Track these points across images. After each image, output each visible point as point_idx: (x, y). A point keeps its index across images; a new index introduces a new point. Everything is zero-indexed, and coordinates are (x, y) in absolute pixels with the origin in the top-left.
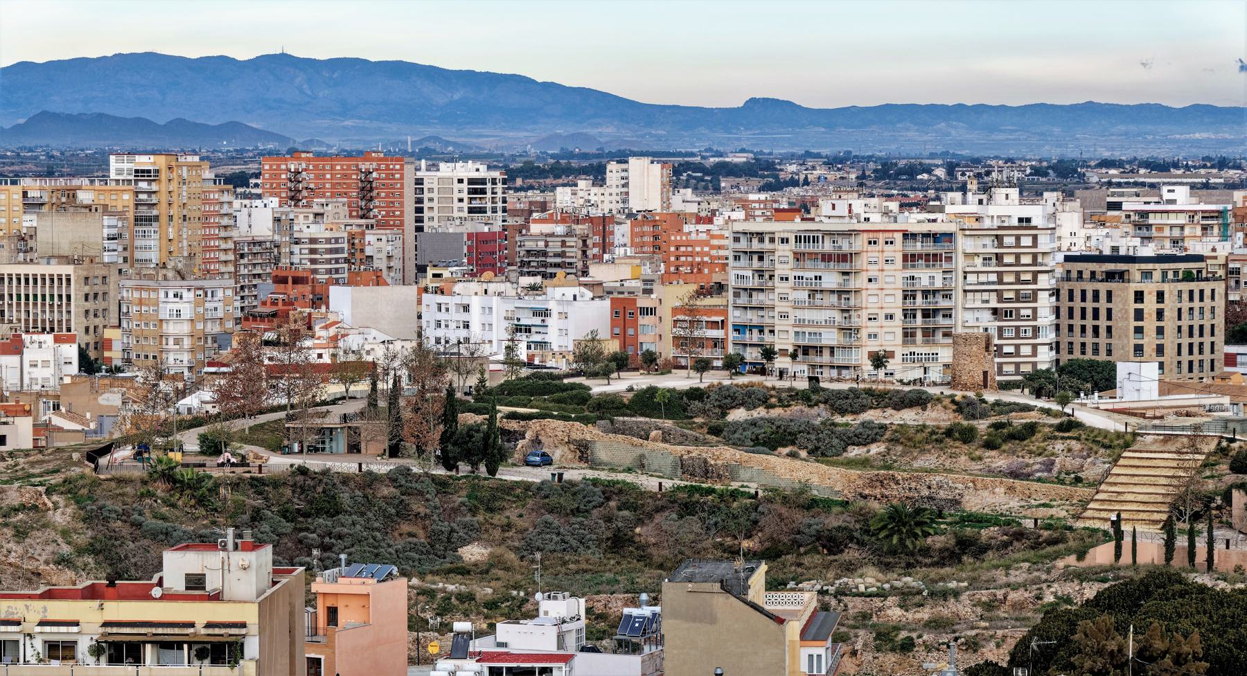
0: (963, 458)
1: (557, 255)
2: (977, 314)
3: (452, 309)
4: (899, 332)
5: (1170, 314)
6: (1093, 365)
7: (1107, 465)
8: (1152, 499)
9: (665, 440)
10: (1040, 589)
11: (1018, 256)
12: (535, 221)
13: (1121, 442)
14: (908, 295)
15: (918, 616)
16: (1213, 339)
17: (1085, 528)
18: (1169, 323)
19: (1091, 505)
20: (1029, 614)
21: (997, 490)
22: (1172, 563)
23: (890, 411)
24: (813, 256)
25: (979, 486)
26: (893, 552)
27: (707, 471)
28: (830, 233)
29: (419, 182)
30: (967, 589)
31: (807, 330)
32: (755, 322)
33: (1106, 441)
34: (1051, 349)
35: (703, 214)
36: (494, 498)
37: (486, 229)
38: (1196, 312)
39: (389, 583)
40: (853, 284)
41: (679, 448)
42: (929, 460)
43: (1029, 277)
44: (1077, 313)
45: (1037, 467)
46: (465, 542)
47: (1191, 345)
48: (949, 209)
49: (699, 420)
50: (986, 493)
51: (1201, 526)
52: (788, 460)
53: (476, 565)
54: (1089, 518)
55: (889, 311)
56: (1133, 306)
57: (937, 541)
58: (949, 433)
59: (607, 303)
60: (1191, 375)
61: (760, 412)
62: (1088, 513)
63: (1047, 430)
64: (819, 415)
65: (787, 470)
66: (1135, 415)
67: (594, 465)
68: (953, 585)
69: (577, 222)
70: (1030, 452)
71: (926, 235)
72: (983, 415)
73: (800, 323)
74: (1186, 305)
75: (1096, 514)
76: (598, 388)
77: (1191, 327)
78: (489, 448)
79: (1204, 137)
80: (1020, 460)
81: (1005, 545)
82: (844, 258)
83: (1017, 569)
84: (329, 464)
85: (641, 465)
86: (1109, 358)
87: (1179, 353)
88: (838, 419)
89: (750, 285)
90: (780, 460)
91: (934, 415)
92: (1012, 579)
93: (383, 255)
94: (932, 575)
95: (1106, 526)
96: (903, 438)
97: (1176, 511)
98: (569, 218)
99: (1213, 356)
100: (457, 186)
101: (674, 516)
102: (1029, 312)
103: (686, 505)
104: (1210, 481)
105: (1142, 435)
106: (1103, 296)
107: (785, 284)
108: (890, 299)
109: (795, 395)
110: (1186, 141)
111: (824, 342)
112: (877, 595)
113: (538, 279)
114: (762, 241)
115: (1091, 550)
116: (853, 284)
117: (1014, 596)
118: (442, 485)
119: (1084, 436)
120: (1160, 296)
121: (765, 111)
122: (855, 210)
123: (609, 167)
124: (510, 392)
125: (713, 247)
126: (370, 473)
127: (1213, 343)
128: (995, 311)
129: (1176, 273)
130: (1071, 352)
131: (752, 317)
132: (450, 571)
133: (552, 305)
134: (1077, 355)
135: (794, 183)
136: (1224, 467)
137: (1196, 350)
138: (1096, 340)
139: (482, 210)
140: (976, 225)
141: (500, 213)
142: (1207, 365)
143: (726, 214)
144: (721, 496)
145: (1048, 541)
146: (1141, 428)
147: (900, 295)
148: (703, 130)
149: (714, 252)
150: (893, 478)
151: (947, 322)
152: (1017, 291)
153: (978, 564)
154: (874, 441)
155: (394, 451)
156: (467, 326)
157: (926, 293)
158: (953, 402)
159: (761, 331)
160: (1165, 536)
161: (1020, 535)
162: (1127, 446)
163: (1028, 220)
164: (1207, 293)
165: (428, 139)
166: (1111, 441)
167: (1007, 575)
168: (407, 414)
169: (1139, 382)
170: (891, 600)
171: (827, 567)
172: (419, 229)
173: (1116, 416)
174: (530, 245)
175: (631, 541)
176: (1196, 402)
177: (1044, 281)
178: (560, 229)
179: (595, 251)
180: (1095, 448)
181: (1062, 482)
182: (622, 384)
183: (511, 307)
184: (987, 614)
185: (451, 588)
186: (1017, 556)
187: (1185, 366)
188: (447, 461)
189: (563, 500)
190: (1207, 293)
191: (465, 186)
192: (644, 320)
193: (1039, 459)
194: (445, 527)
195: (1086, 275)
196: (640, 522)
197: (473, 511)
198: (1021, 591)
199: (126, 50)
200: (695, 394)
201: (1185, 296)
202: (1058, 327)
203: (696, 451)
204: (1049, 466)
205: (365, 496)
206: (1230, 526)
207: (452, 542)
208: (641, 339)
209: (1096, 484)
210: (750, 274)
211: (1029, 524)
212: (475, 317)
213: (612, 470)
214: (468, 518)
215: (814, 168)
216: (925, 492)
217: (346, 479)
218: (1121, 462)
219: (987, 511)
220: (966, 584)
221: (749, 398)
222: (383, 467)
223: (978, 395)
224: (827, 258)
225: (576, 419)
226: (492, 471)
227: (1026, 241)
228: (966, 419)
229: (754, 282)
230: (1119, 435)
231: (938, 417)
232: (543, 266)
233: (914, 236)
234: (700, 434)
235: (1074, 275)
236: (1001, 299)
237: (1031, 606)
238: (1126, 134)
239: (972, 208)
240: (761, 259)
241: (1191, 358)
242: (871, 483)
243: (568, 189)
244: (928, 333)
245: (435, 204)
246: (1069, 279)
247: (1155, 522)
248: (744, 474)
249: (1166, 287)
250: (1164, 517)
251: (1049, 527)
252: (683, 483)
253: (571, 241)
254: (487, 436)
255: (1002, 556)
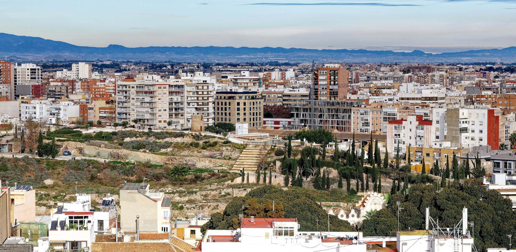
0: (196, 152)
1: (58, 92)
2: (191, 109)
3: (31, 108)
4: (168, 115)
5: (247, 109)
8: (252, 164)
9: (105, 147)
11: (203, 92)
12: (52, 81)
14: (171, 104)
15: (184, 199)
18: (247, 112)
23: (173, 138)
24: (142, 92)
26: (176, 180)
27: (119, 157)
28: (147, 85)
29: (15, 69)
31: (140, 114)
32: (124, 112)
35: (102, 79)
36: (54, 165)
37: (37, 84)
38: (255, 109)
39: (30, 191)
40: (154, 100)
41: (110, 150)
42: (186, 153)
43: (206, 98)
44: (220, 109)
46: (46, 179)
47: (254, 118)
48: (182, 78)
49: (116, 141)
52: (143, 153)
53: (49, 185)
55: (165, 109)
56: (237, 107)
57: (189, 177)
58: (191, 144)
59: (78, 106)
61: (134, 139)
64: (152, 139)
65: (143, 156)
67: (84, 155)
68: (195, 190)
69: (65, 82)
70: (216, 150)
71: (175, 86)
72: (201, 139)
73: (138, 112)
74: (252, 106)
76: (84, 132)
77: (254, 113)
78: (50, 150)
79: (246, 57)
81: (210, 178)
82: (151, 93)
84: (4, 155)
85: (98, 155)
88: (158, 141)
89: (123, 101)
90: (141, 153)
91: (186, 139)
92: (212, 188)
93: (5, 92)
94: (188, 187)
95: (239, 172)
96: (177, 146)
98: (62, 80)
100: (27, 71)
101: (110, 170)
102: (206, 109)
103: (113, 167)
106: (228, 104)
107: (133, 100)
108: (165, 105)
109: (144, 134)
110: (240, 58)
111: (145, 118)
112: (172, 193)
113: (54, 99)
114: (126, 87)
116: (154, 100)
118: (38, 161)
120: (245, 104)
121: (114, 48)
122: (154, 78)
123: (73, 65)
124: (58, 133)
125: (107, 89)
126: (16, 158)
128: (196, 108)
129: (249, 97)
131: (123, 110)
132: (42, 187)
133: (61, 107)
134: (220, 121)
135: (125, 70)
136: (273, 154)
137: (255, 120)
139: (35, 78)
140: (190, 83)
141: (40, 79)
143: (109, 80)
144: (124, 164)
145: (222, 177)
147: (168, 104)
148: (96, 54)
149: (107, 91)
150: (175, 158)
151: (182, 112)
152: (203, 102)
154: (169, 147)
155: (23, 151)
156: (35, 113)
157: (176, 103)
158: (192, 135)
159: (126, 115)
161: (214, 175)
162: (244, 148)
163: (206, 81)
164: (258, 103)
165: (12, 57)
168: (26, 140)
169: (242, 129)
170: (176, 195)
171: (157, 185)
172: (15, 84)
174: (51, 89)
175: (96, 178)
177: (211, 100)
178: (59, 84)
179: (70, 90)
182: (92, 131)
183: (49, 107)
185: (42, 192)
187: (252, 124)
188: (40, 155)
189: (77, 166)
190: (258, 103)
191: (29, 71)
192: (89, 111)
193: (218, 152)
194: (40, 174)
195: (223, 98)
196: (99, 172)
197: (48, 169)
198: (215, 191)
199: (27, 35)
200: (114, 134)
201: (252, 104)
202: (214, 113)
203: (115, 151)
205: (15, 165)
206: (275, 171)
207: (42, 179)
208: (89, 117)
209: (235, 160)
210: (123, 97)
211: (216, 171)
212: (38, 111)
213: (90, 156)
214: (47, 171)
215: (131, 66)
216: (185, 162)
217: (9, 160)
218: (243, 153)
219: (203, 168)
221: (131, 134)
222: (20, 156)
224: (146, 92)
225: (78, 141)
226: (53, 157)
227: (205, 88)
229: (124, 100)
230: (242, 145)
231: (188, 140)
232: (56, 96)
233: (172, 86)
234: (117, 145)
235: (219, 97)
236: (198, 105)
238: (222, 55)
239: (189, 77)
240: (126, 93)
242: (168, 160)
243: (60, 72)
244: (176, 115)
245: (20, 76)
246: (217, 99)
247: (254, 171)
248: (130, 157)
249: (246, 101)
250: (256, 169)
251: (222, 172)
252: (112, 160)
253: (63, 88)
254: (51, 147)
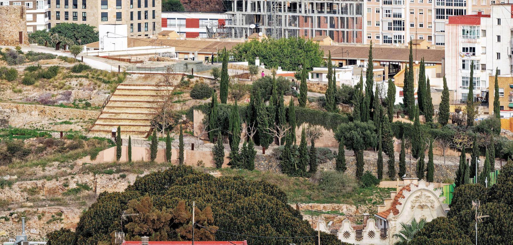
6: (74, 27)
7: (107, 95)
8: (139, 117)
10: (67, 179)
13: (116, 79)
16: (154, 9)
17: (95, 138)
19: (98, 122)
20: (60, 197)
21: (33, 113)
22: (156, 160)
25: (21, 110)
30: (17, 180)
33: (105, 78)
34: (46, 17)
45: (59, 96)
47: (139, 13)
50: (25, 115)
51: (174, 135)
54: (97, 131)
60: (140, 33)
62: (96, 128)
63: (65, 71)
66: (123, 60)
68: (7, 178)
70: (54, 87)
72: (21, 62)
75: (102, 128)
80: (48, 92)
81: (41, 150)
83: (50, 166)
86: (84, 22)
87: (132, 19)
92: (47, 173)
95: (109, 136)
97: (156, 124)
99: (154, 20)
104: (178, 105)
105: (130, 74)
115: (100, 153)
117: (49, 185)
119: (90, 75)
127: (154, 11)
130: (58, 18)
134: (62, 20)
136: (187, 95)
137: (143, 16)
138: (75, 10)
142: (150, 26)
145: (70, 147)
146: (129, 70)
153: (23, 163)
160: (151, 142)
161: (51, 143)
162: (120, 81)
166: (109, 78)
167: (44, 170)
169: (114, 39)
173: (111, 61)
176: (153, 51)
180: (99, 83)
181: (77, 107)
184: (31, 197)
186: (50, 157)
187: (136, 27)
193: (61, 91)
198: (54, 180)
204: (68, 96)
206: (192, 134)
209: (100, 108)
218: (117, 92)
219: (27, 127)
220: (16, 177)
223: (18, 48)
228: (9, 64)
230: (114, 74)
237: (61, 191)
241: (139, 21)
250: (148, 129)
251: (70, 137)
255: (39, 158)
